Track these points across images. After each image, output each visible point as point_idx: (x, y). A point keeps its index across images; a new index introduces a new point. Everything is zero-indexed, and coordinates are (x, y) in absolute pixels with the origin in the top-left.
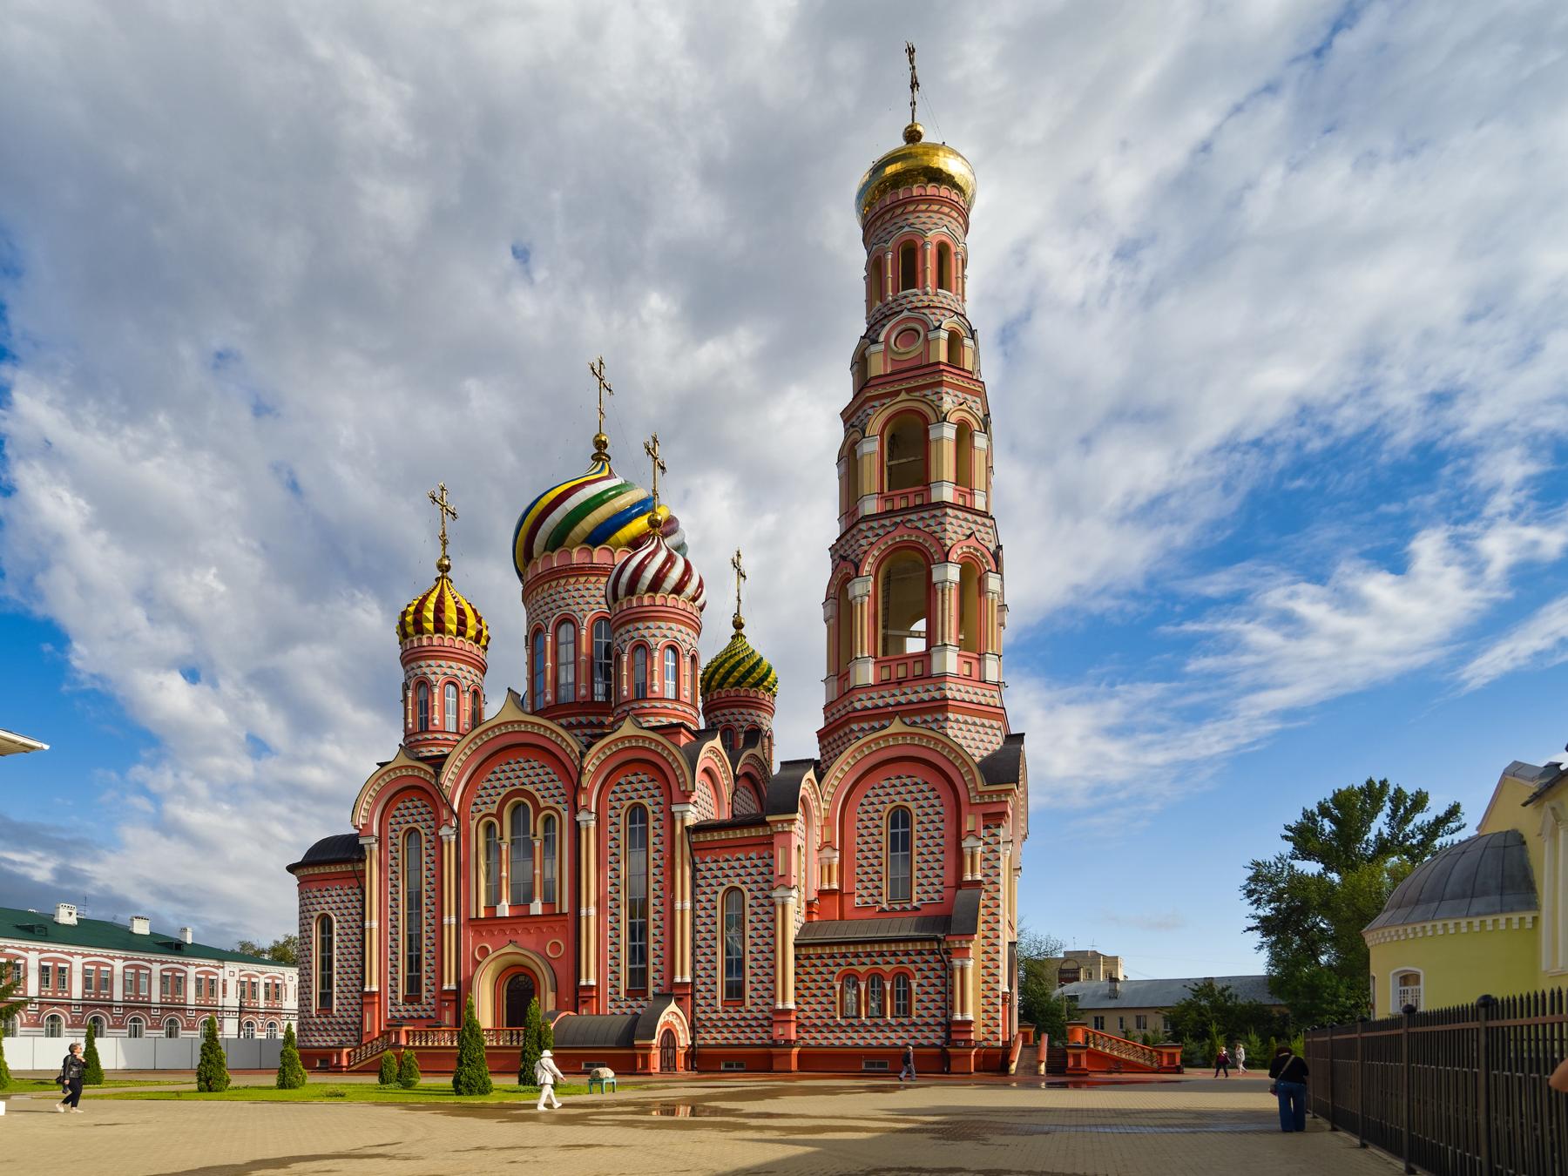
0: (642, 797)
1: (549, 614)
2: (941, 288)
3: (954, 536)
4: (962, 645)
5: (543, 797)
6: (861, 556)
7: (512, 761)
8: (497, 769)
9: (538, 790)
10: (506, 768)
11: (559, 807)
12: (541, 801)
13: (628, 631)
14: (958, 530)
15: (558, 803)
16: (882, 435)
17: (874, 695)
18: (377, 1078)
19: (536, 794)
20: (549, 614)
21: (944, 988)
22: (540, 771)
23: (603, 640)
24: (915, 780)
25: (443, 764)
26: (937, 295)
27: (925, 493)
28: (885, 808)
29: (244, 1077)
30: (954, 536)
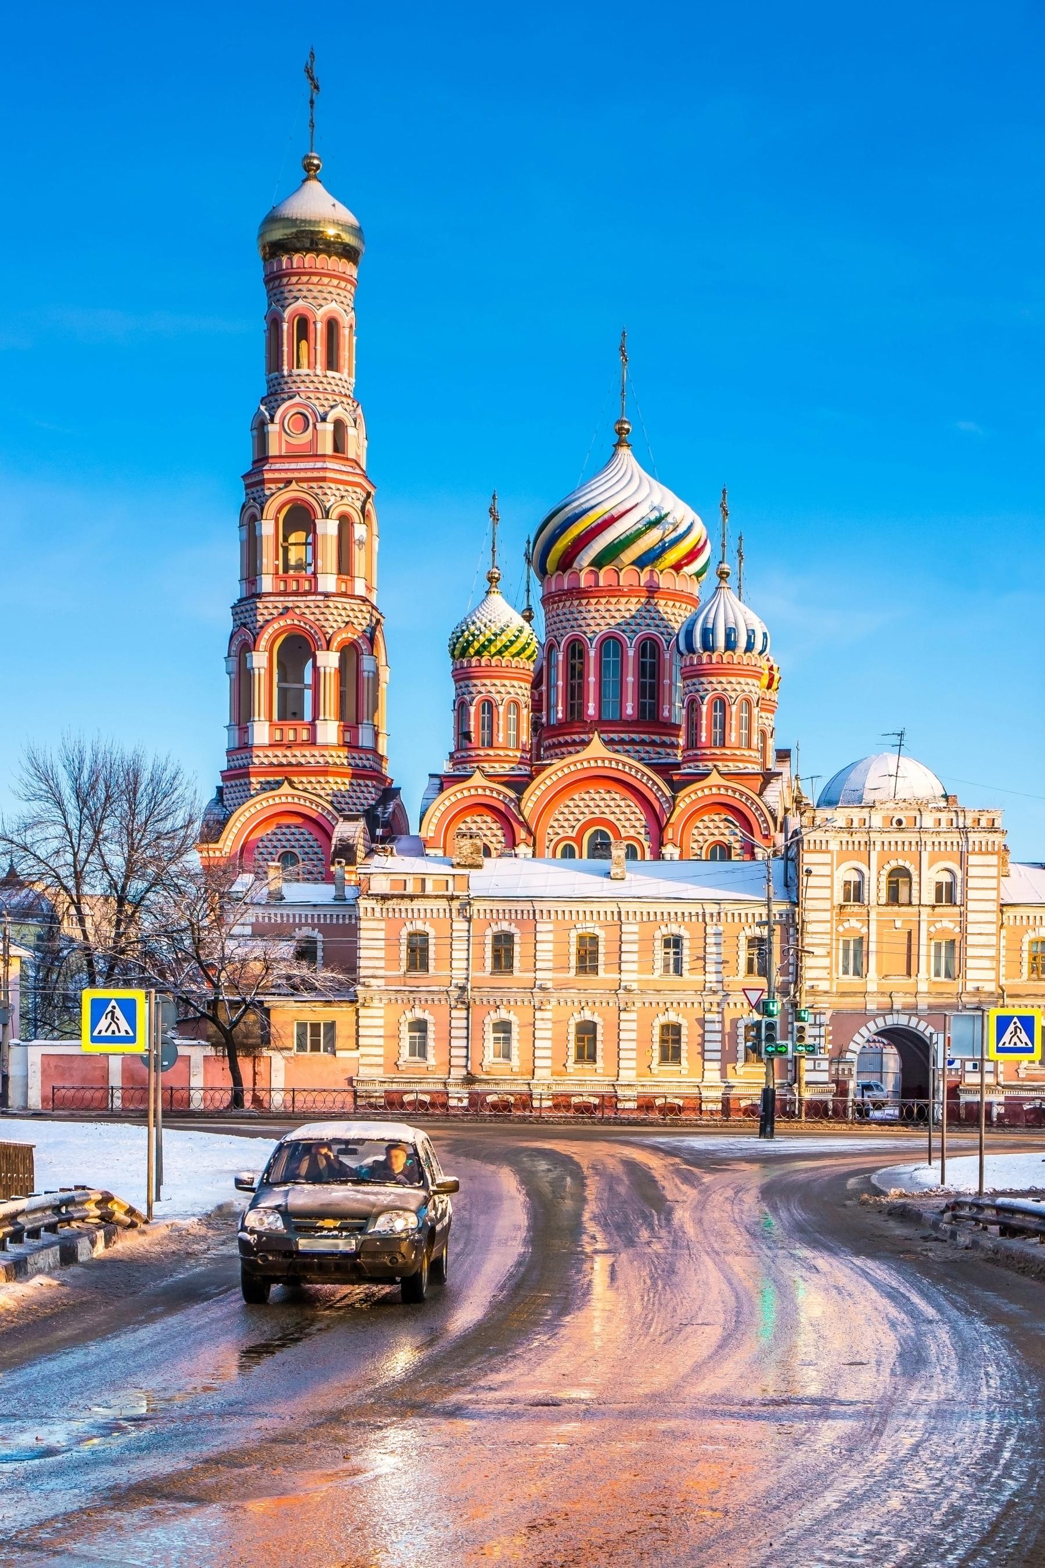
3: (335, 625)
4: (341, 716)
5: (624, 826)
7: (592, 791)
8: (576, 797)
9: (619, 820)
11: (641, 838)
12: (622, 830)
13: (694, 684)
14: (339, 619)
15: (639, 833)
16: (277, 520)
17: (270, 754)
18: (80, 1240)
19: (617, 823)
21: (764, 980)
22: (622, 803)
23: (611, 659)
24: (302, 830)
25: (528, 785)
26: (326, 376)
27: (349, 583)
30: (335, 625)
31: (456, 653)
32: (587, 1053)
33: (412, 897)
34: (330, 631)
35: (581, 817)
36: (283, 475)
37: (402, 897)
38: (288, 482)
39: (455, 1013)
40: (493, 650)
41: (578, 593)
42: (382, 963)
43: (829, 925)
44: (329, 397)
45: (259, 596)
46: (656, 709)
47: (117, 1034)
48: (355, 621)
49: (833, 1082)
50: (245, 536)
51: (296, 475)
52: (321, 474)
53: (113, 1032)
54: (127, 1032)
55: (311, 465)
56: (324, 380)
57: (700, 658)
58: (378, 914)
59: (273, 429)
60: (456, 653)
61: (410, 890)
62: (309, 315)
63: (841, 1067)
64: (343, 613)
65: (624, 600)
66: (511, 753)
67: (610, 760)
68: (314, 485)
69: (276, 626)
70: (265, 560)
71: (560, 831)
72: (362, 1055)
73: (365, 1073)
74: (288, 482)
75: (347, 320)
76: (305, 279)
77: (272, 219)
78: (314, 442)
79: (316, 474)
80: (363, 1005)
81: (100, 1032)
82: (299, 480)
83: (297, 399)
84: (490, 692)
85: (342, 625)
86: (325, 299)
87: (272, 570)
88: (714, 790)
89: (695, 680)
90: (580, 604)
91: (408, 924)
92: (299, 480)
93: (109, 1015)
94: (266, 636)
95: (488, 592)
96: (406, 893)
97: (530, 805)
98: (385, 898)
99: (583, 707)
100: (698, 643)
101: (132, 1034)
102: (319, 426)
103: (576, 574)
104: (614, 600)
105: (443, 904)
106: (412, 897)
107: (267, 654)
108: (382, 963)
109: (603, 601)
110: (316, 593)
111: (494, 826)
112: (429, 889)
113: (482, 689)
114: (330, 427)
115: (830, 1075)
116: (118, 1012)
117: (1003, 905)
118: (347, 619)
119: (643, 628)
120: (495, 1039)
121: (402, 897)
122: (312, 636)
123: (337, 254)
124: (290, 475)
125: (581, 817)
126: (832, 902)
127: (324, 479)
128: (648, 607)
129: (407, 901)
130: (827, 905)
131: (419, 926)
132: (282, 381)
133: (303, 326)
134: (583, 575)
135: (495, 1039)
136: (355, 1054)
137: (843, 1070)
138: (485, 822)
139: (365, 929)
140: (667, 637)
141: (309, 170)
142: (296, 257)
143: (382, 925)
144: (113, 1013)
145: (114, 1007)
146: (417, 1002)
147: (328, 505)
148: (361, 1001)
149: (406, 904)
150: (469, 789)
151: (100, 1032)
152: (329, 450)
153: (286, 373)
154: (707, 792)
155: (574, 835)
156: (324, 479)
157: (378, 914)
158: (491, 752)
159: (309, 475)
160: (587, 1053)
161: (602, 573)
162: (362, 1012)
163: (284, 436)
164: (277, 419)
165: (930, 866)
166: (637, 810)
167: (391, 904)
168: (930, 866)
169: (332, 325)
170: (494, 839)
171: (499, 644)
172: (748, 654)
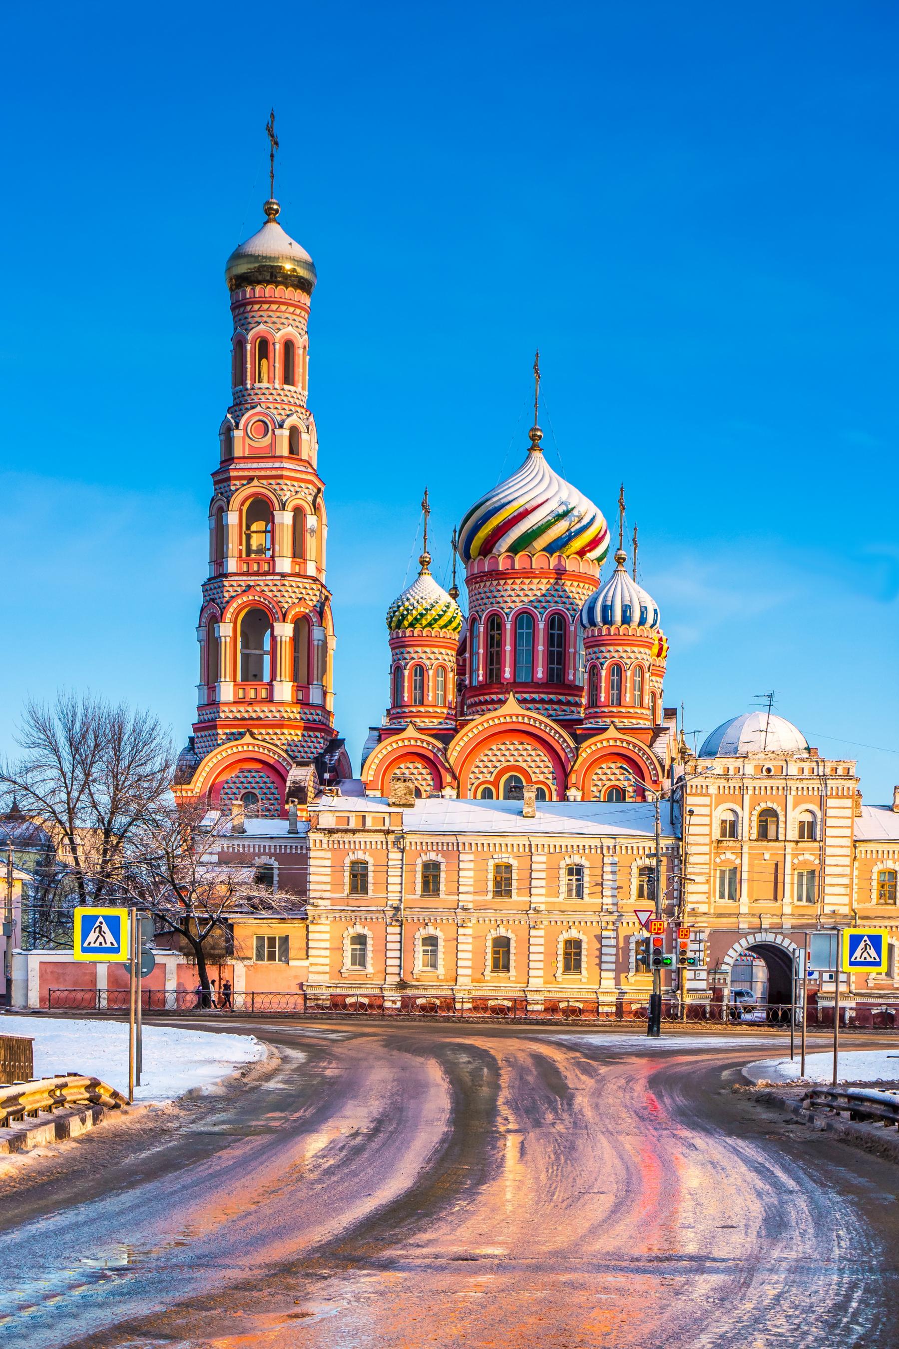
0: (253, 788)
1: (483, 607)
2: (288, 384)
3: (289, 600)
4: (295, 678)
5: (534, 773)
6: (224, 605)
8: (494, 747)
9: (530, 767)
10: (503, 747)
11: (549, 782)
12: (533, 776)
15: (547, 778)
19: (529, 770)
20: (483, 607)
22: (533, 753)
23: (525, 631)
24: (261, 774)
26: (283, 389)
28: (240, 792)
29: (700, 1046)
30: (289, 600)
31: (393, 625)
32: (501, 963)
33: (354, 832)
34: (286, 606)
35: (498, 764)
36: (246, 473)
37: (346, 831)
38: (251, 479)
39: (390, 929)
40: (424, 622)
41: (498, 575)
42: (328, 887)
43: (708, 857)
44: (286, 407)
45: (226, 575)
46: (562, 673)
47: (104, 945)
48: (307, 597)
49: (710, 989)
50: (213, 525)
51: (258, 473)
52: (279, 473)
53: (101, 944)
54: (112, 944)
55: (270, 465)
56: (281, 392)
57: (600, 630)
58: (325, 846)
59: (238, 434)
60: (393, 625)
61: (353, 825)
62: (269, 337)
63: (717, 976)
64: (297, 590)
65: (536, 581)
66: (438, 710)
67: (523, 716)
68: (273, 482)
69: (240, 601)
70: (230, 545)
71: (480, 776)
72: (311, 964)
73: (313, 979)
74: (251, 479)
75: (301, 341)
76: (265, 306)
77: (238, 256)
78: (273, 445)
79: (274, 473)
80: (312, 922)
81: (89, 943)
82: (260, 478)
83: (258, 409)
84: (421, 658)
85: (296, 601)
86: (283, 324)
87: (236, 554)
88: (612, 743)
89: (596, 649)
90: (499, 584)
91: (350, 853)
92: (260, 478)
93: (98, 929)
94: (231, 610)
95: (420, 574)
96: (349, 827)
97: (455, 754)
98: (331, 832)
99: (501, 671)
100: (598, 618)
101: (116, 945)
102: (277, 432)
103: (495, 559)
104: (527, 581)
105: (380, 837)
106: (354, 832)
107: (232, 625)
108: (328, 887)
109: (518, 581)
110: (274, 574)
111: (424, 771)
112: (369, 825)
113: (415, 656)
114: (286, 433)
115: (708, 983)
116: (105, 927)
117: (856, 841)
118: (300, 596)
119: (552, 604)
120: (424, 951)
121: (346, 831)
122: (270, 610)
123: (293, 286)
124: (252, 473)
125: (498, 764)
126: (711, 838)
127: (281, 477)
128: (514, 586)
129: (350, 835)
130: (706, 840)
131: (360, 855)
132: (245, 393)
133: (264, 347)
134: (501, 559)
135: (424, 951)
136: (306, 963)
137: (719, 979)
138: (417, 768)
139: (314, 858)
140: (573, 613)
141: (270, 214)
142: (258, 288)
143: (329, 854)
144: (100, 928)
145: (101, 923)
146: (358, 920)
147: (284, 499)
148: (310, 919)
149: (349, 837)
150: (403, 740)
151: (89, 943)
152: (286, 453)
153: (249, 386)
154: (605, 743)
155: (492, 779)
156: (281, 477)
157: (325, 846)
158: (422, 709)
159: (268, 473)
160: (501, 963)
161: (517, 558)
162: (311, 928)
163: (248, 440)
164: (241, 426)
165: (794, 807)
166: (546, 759)
167: (336, 836)
168: (794, 807)
169: (289, 346)
170: (424, 783)
171: (429, 618)
172: (641, 627)
